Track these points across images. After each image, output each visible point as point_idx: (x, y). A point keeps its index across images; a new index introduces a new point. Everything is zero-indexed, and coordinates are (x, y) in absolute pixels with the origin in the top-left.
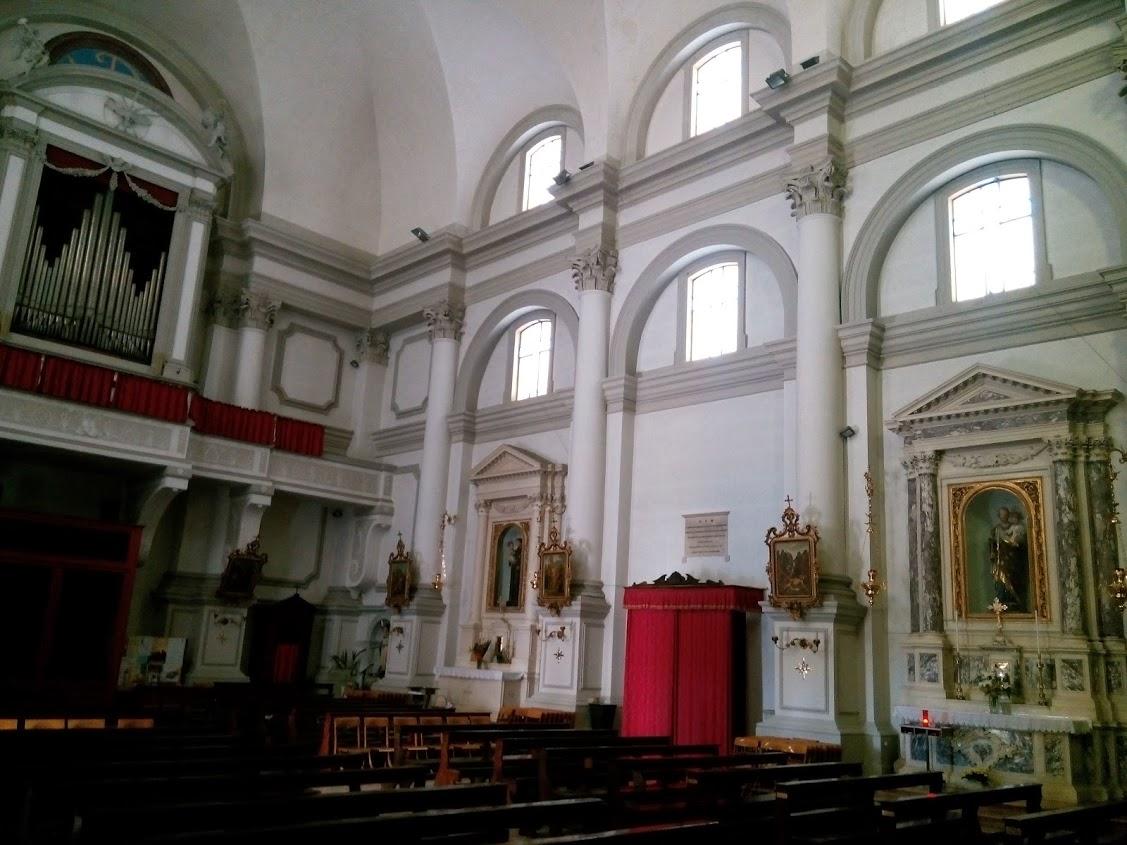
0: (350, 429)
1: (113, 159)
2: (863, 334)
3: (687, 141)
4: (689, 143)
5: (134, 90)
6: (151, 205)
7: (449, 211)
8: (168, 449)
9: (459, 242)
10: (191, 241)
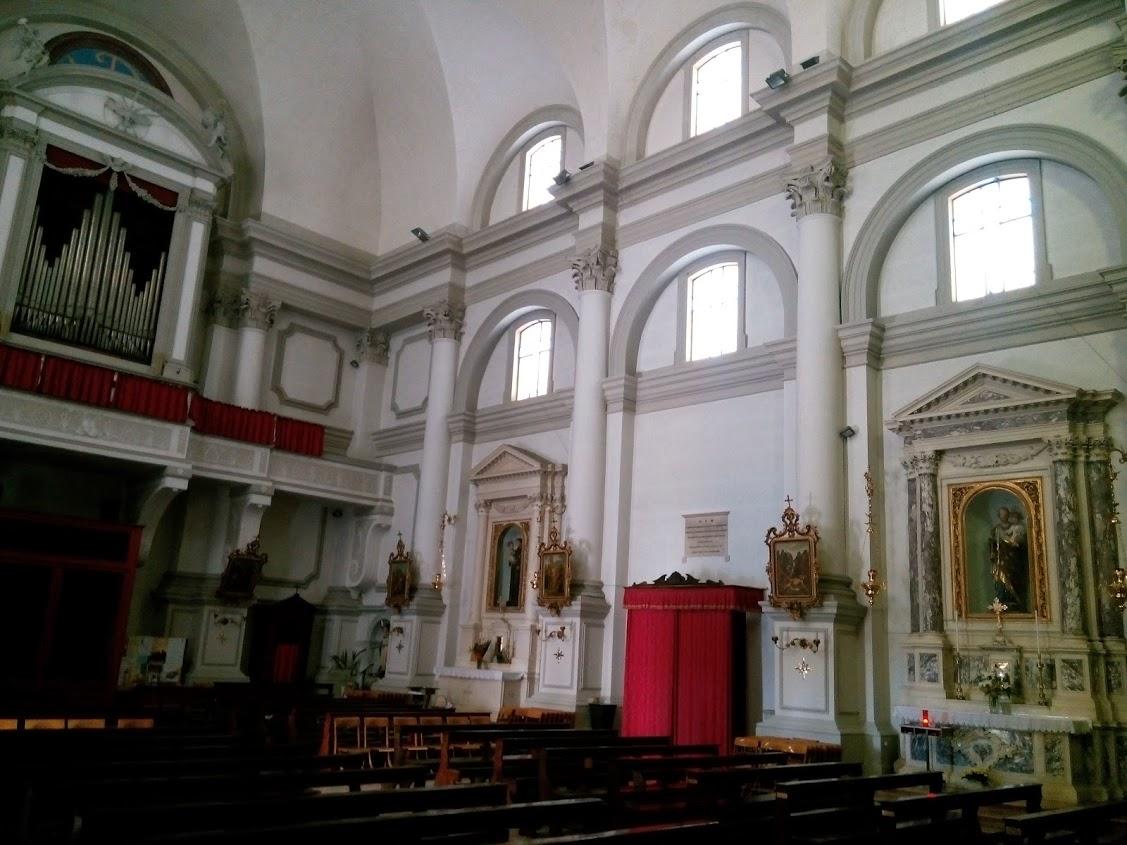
0: (350, 429)
1: (113, 159)
2: (863, 334)
3: (687, 141)
4: (689, 143)
5: (134, 90)
6: (151, 205)
7: (449, 211)
8: (168, 449)
9: (459, 242)
10: (191, 241)
